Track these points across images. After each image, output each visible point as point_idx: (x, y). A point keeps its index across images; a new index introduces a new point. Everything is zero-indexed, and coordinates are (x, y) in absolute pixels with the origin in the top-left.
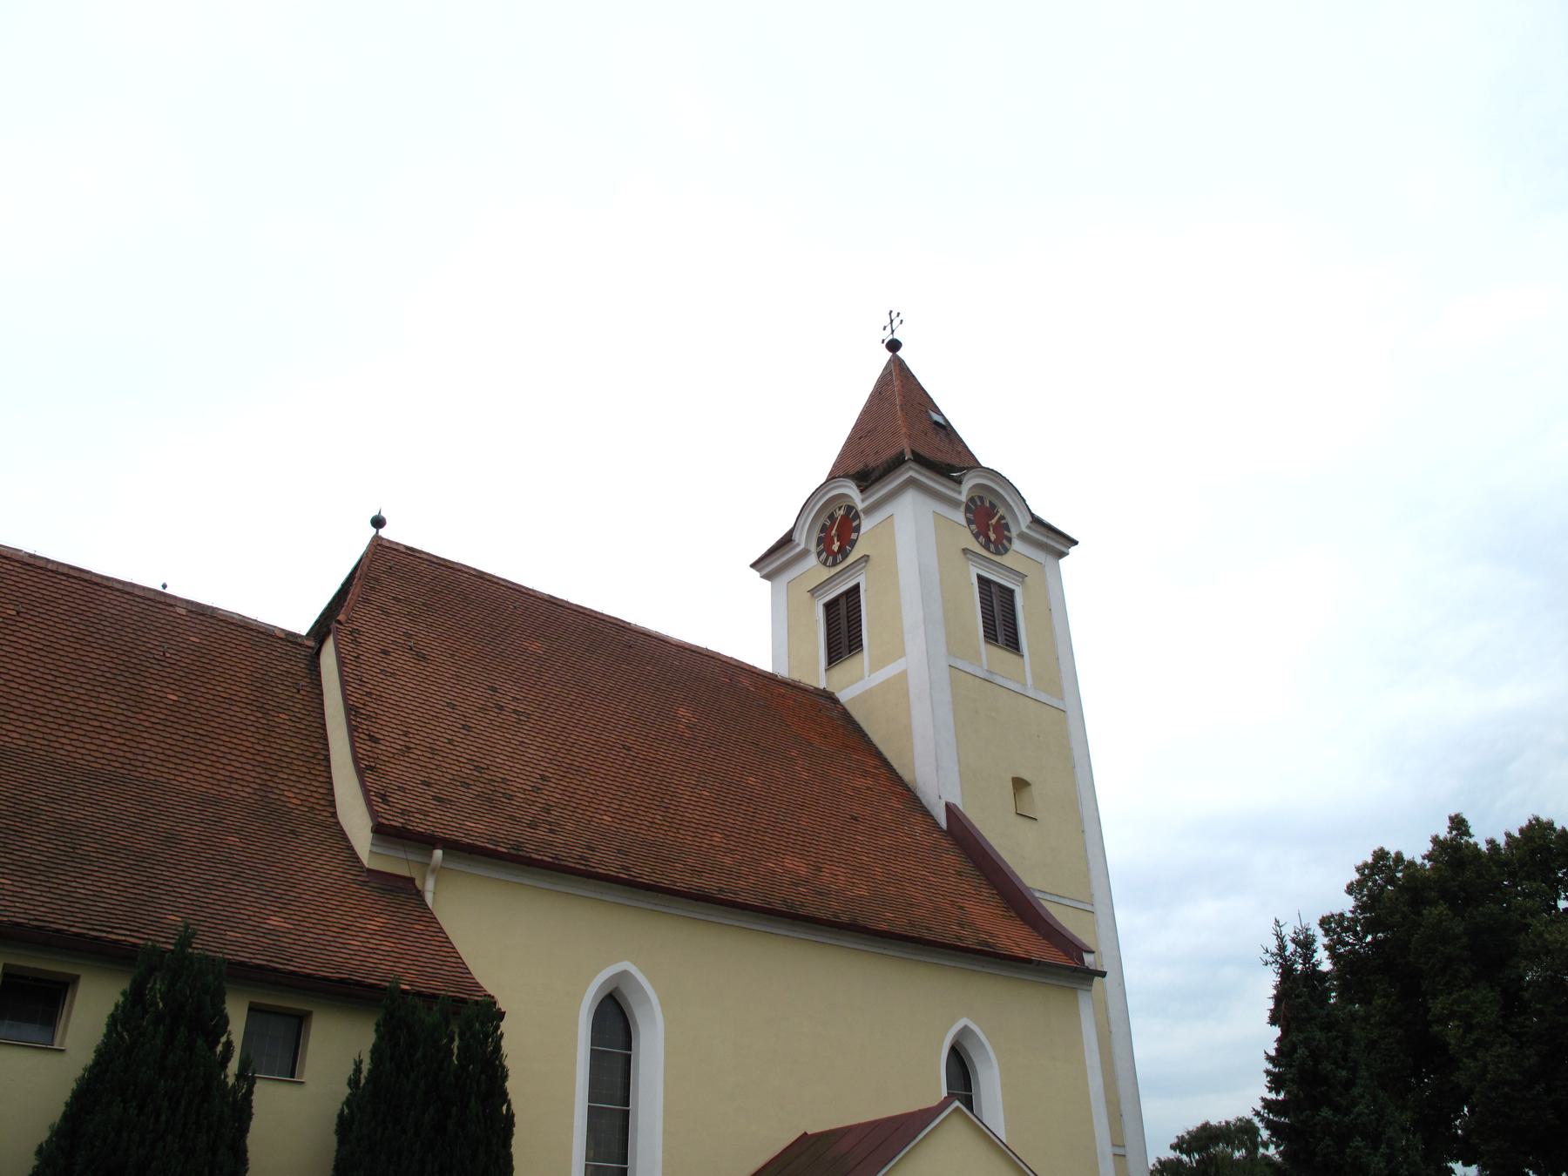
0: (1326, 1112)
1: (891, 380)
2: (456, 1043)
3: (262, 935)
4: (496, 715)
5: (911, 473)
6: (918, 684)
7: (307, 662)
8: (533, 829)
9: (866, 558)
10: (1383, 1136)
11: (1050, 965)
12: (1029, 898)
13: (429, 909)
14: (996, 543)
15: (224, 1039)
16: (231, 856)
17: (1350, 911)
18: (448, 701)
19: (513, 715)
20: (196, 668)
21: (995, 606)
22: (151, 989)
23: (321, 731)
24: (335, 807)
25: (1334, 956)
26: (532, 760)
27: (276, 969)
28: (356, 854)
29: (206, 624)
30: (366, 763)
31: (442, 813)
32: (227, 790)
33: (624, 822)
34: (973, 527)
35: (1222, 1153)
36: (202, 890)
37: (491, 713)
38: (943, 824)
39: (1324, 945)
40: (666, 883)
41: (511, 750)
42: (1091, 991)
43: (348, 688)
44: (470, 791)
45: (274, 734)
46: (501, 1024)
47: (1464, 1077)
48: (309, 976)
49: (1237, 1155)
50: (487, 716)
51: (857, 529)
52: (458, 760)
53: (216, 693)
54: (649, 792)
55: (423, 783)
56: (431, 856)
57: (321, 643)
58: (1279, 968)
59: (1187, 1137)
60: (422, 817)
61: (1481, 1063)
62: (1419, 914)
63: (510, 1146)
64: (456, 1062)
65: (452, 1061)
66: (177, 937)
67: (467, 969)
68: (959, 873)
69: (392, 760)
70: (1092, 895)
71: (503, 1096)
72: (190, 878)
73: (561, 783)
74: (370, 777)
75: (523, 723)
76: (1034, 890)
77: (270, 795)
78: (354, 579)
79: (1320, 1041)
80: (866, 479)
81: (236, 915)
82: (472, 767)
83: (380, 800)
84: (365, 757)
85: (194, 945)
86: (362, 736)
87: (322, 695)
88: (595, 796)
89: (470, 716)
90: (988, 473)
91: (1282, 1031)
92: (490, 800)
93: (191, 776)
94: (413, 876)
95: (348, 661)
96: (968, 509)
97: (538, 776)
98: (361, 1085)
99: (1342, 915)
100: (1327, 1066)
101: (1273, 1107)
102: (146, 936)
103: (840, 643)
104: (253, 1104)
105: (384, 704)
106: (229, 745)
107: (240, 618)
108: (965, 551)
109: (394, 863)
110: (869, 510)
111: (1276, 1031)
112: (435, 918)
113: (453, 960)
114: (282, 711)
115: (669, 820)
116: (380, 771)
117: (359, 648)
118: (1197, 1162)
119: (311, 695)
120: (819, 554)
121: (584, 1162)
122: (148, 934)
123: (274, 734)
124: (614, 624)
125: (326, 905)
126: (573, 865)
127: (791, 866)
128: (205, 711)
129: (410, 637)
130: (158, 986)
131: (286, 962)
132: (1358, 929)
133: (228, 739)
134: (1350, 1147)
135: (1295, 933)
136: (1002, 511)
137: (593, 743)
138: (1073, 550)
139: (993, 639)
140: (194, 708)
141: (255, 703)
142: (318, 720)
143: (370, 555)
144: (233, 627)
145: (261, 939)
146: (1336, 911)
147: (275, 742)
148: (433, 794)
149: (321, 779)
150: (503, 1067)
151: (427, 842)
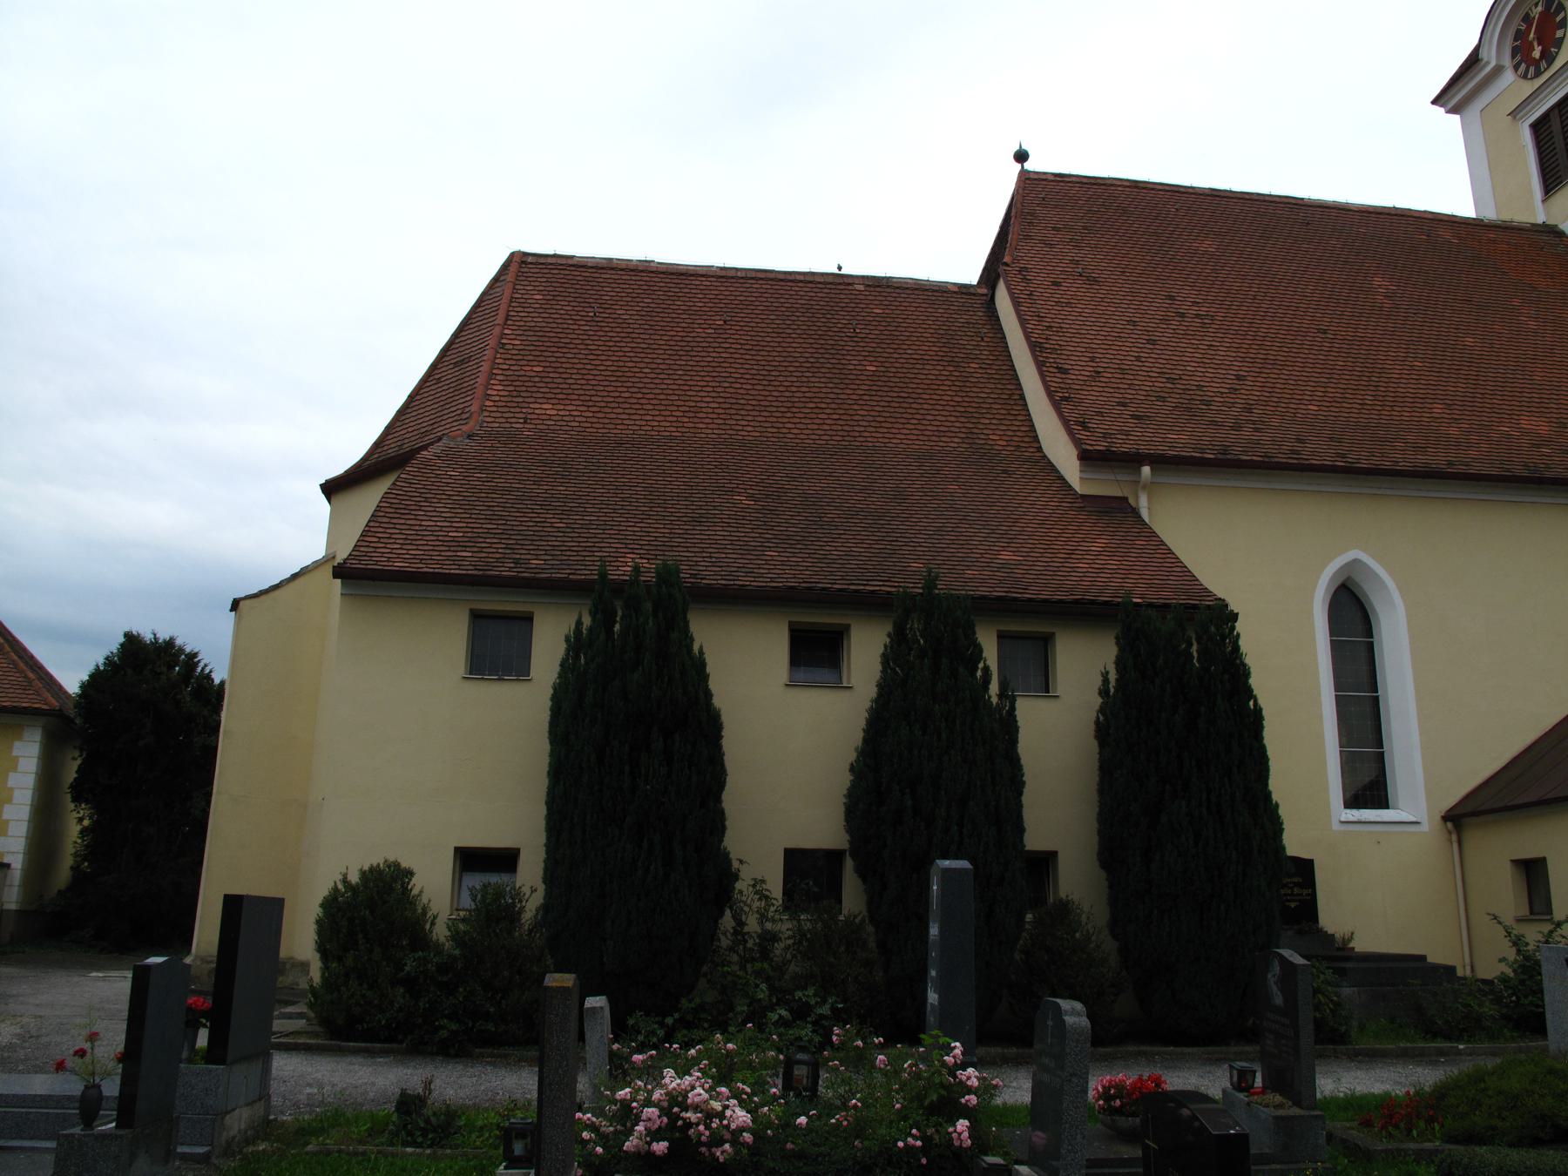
2: (1195, 647)
13: (1146, 524)
15: (981, 665)
24: (1039, 442)
27: (1015, 599)
28: (1067, 482)
40: (1387, 464)
44: (1166, 404)
45: (968, 384)
50: (1170, 326)
55: (1119, 404)
56: (1139, 472)
57: (993, 288)
60: (1124, 437)
63: (1262, 738)
64: (1197, 665)
66: (923, 581)
69: (1085, 387)
71: (1249, 693)
75: (1208, 326)
82: (1164, 380)
83: (1080, 428)
85: (939, 587)
86: (1051, 369)
98: (1111, 694)
102: (896, 584)
104: (1018, 719)
109: (1105, 485)
112: (1154, 532)
113: (1179, 569)
115: (1381, 398)
117: (1031, 285)
119: (994, 340)
120: (1516, 68)
123: (968, 384)
126: (1284, 460)
130: (915, 625)
143: (1021, 191)
145: (997, 574)
151: (1132, 461)
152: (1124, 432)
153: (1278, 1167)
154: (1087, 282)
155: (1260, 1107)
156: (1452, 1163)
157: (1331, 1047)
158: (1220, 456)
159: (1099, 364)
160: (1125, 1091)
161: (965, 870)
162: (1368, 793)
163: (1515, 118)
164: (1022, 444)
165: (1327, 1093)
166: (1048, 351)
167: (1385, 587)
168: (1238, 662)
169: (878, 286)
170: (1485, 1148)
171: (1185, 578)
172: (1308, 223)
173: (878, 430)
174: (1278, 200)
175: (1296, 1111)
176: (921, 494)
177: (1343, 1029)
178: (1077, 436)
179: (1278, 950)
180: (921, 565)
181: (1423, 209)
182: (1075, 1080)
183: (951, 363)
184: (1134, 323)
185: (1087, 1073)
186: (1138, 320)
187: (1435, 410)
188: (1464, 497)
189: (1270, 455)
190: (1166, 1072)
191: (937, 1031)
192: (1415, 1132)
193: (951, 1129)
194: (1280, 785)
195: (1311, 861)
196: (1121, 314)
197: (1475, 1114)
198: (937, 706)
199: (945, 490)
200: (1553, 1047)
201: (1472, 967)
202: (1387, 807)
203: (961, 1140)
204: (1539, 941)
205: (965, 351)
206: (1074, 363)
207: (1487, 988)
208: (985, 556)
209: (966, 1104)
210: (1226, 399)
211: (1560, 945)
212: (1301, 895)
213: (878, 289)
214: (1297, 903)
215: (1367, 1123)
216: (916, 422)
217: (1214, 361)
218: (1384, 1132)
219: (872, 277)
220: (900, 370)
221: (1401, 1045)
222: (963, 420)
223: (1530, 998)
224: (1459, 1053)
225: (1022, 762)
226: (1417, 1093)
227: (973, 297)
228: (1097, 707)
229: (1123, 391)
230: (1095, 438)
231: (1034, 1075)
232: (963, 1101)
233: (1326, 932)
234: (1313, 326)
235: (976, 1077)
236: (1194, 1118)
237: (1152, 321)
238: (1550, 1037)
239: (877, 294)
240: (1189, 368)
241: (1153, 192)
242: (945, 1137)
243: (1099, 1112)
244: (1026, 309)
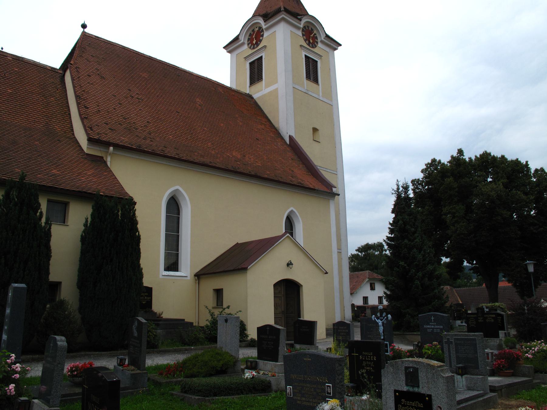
0: (406, 241)
5: (283, 16)
6: (281, 93)
7: (60, 79)
8: (145, 140)
9: (265, 47)
10: (423, 249)
13: (109, 167)
15: (39, 211)
17: (422, 178)
18: (113, 94)
19: (137, 100)
21: (310, 67)
22: (12, 194)
23: (67, 104)
24: (73, 132)
25: (415, 192)
27: (56, 188)
30: (84, 116)
32: (33, 125)
35: (372, 252)
37: (129, 99)
38: (288, 142)
39: (412, 189)
41: (137, 112)
42: (334, 200)
43: (76, 88)
44: (122, 126)
46: (135, 206)
47: (450, 232)
48: (68, 190)
49: (376, 253)
51: (263, 36)
52: (117, 116)
53: (26, 90)
55: (105, 123)
56: (109, 149)
57: (65, 71)
58: (396, 195)
60: (105, 135)
61: (456, 228)
62: (444, 180)
63: (139, 246)
64: (120, 219)
65: (119, 218)
66: (20, 177)
67: (123, 188)
68: (292, 159)
69: (94, 115)
70: (337, 169)
71: (137, 230)
73: (155, 124)
74: (86, 121)
75: (141, 102)
78: (76, 48)
79: (407, 219)
80: (267, 17)
81: (40, 169)
82: (123, 118)
83: (90, 129)
84: (84, 114)
85: (26, 179)
87: (66, 91)
89: (121, 100)
90: (312, 17)
91: (395, 215)
94: (103, 156)
96: (303, 31)
97: (146, 122)
99: (419, 179)
100: (408, 227)
101: (390, 239)
102: (9, 176)
103: (255, 77)
104: (52, 232)
105: (89, 95)
106: (33, 109)
107: (33, 62)
108: (301, 46)
109: (96, 151)
110: (267, 29)
111: (393, 215)
113: (118, 185)
118: (364, 255)
119: (62, 91)
120: (248, 44)
122: (9, 176)
124: (173, 67)
126: (159, 153)
127: (235, 155)
128: (23, 97)
129: (98, 70)
131: (59, 185)
132: (423, 184)
133: (32, 107)
134: (412, 252)
136: (315, 32)
137: (166, 110)
138: (339, 48)
139: (309, 79)
140: (18, 95)
141: (41, 94)
142: (66, 100)
143: (81, 39)
144: (31, 65)
146: (417, 178)
147: (50, 108)
149: (67, 122)
151: (107, 144)
152: (105, 134)
153: (131, 391)
154: (101, 78)
155: (126, 371)
157: (152, 349)
158: (137, 148)
159: (100, 108)
160: (79, 368)
161: (23, 288)
162: (172, 266)
163: (245, 59)
165: (149, 365)
166: (82, 99)
169: (18, 60)
170: (196, 378)
173: (9, 116)
174: (171, 66)
175: (139, 371)
176: (24, 143)
177: (156, 344)
178: (88, 132)
179: (137, 318)
180: (20, 170)
181: (215, 80)
182: (59, 365)
183: (43, 96)
184: (115, 96)
185: (65, 363)
186: (117, 95)
187: (209, 145)
189: (154, 150)
192: (176, 375)
193: (7, 389)
194: (144, 262)
195: (152, 288)
198: (19, 225)
199: (34, 143)
200: (218, 346)
202: (178, 271)
203: (11, 392)
204: (218, 314)
205: (50, 93)
206: (91, 105)
208: (46, 170)
209: (14, 378)
210: (143, 129)
211: (224, 315)
212: (147, 299)
215: (161, 374)
216: (26, 115)
218: (166, 376)
219: (16, 55)
221: (174, 348)
222: (45, 118)
224: (192, 349)
225: (52, 248)
226: (177, 363)
227: (56, 73)
228: (82, 230)
229: (108, 119)
230: (94, 134)
231: (44, 365)
232: (13, 377)
233: (154, 312)
234: (175, 110)
235: (20, 367)
236: (102, 376)
238: (218, 343)
239: (17, 63)
242: (4, 392)
243: (68, 377)
244: (76, 82)
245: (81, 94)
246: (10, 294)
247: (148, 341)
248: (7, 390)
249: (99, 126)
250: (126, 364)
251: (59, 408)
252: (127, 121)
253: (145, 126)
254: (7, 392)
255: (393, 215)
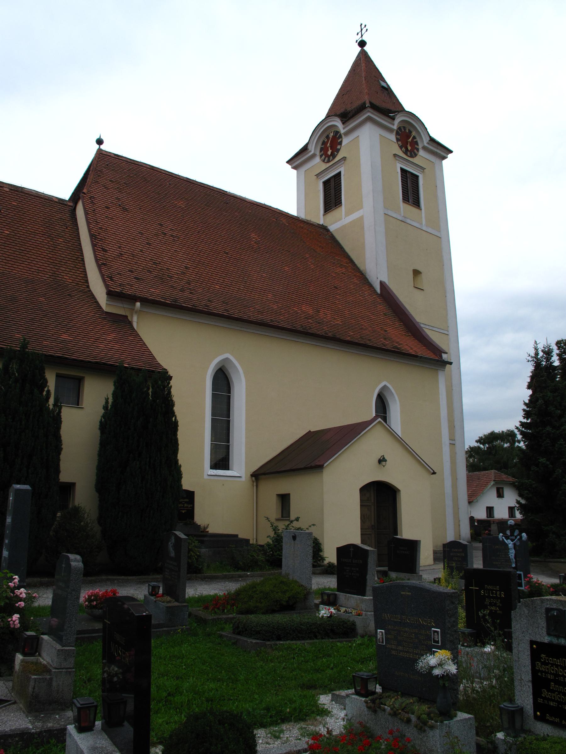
0: (549, 428)
1: (360, 63)
2: (151, 390)
3: (59, 343)
4: (163, 238)
5: (369, 114)
6: (368, 222)
9: (344, 159)
11: (426, 358)
12: (418, 327)
13: (135, 330)
14: (410, 151)
15: (46, 389)
16: (42, 307)
20: (17, 218)
23: (79, 247)
25: (561, 359)
26: (181, 259)
27: (67, 358)
28: (99, 305)
29: (19, 196)
31: (139, 285)
32: (37, 276)
33: (225, 289)
34: (400, 143)
36: (30, 323)
37: (160, 237)
38: (379, 291)
39: (557, 354)
40: (245, 317)
41: (170, 255)
44: (152, 274)
45: (57, 249)
48: (82, 361)
49: (506, 445)
50: (158, 238)
51: (340, 143)
54: (237, 274)
56: (135, 305)
57: (76, 204)
58: (534, 363)
59: (483, 437)
60: (130, 287)
63: (177, 435)
66: (20, 344)
67: (154, 357)
68: (385, 314)
69: (114, 260)
72: (24, 318)
74: (104, 269)
76: (421, 323)
77: (57, 278)
80: (345, 117)
82: (152, 263)
83: (109, 279)
85: (29, 348)
86: (99, 249)
87: (78, 229)
88: (212, 276)
91: (532, 392)
92: (161, 279)
93: (20, 270)
95: (90, 213)
96: (397, 133)
98: (109, 409)
102: (7, 344)
103: (331, 201)
107: (36, 192)
108: (395, 155)
109: (118, 309)
111: (530, 392)
112: (138, 334)
113: (148, 353)
114: (60, 238)
115: (247, 288)
116: (108, 265)
117: (95, 206)
118: (487, 448)
120: (321, 156)
121: (210, 442)
123: (57, 249)
125: (87, 329)
126: (202, 309)
128: (23, 239)
129: (119, 200)
130: (14, 367)
133: (35, 252)
135: (544, 347)
136: (414, 134)
138: (450, 156)
139: (407, 201)
140: (17, 237)
143: (97, 159)
144: (33, 197)
145: (59, 345)
148: (134, 276)
150: (172, 401)
151: (132, 299)
155: (160, 602)
156: (239, 622)
157: (195, 575)
160: (99, 597)
163: (317, 177)
164: (79, 283)
165: (191, 595)
166: (99, 239)
167: (239, 372)
168: (170, 399)
170: (253, 615)
171: (150, 357)
172: (227, 203)
175: (176, 604)
176: (25, 300)
177: (200, 567)
178: (107, 283)
179: (174, 532)
180: (21, 336)
184: (142, 234)
185: (80, 589)
188: (225, 326)
189: (196, 305)
190: (119, 588)
191: (6, 570)
192: (226, 611)
193: (10, 619)
194: (183, 457)
195: (193, 492)
196: (136, 228)
197: (250, 602)
200: (283, 573)
201: (256, 540)
202: (228, 469)
203: (15, 625)
204: (284, 529)
207: (261, 548)
209: (18, 606)
210: (180, 277)
213: (16, 193)
214: (186, 511)
215: (206, 608)
217: (176, 258)
218: (213, 611)
220: (22, 236)
221: (224, 573)
223: (278, 552)
224: (248, 576)
225: (62, 438)
226: (228, 593)
230: (116, 286)
231: (54, 591)
232: (17, 605)
235: (25, 593)
237: (100, 218)
240: (164, 259)
241: (160, 173)
243: (86, 608)
244: (91, 217)
245: (98, 232)
246: (11, 498)
247: (188, 563)
248: (10, 621)
249: (122, 275)
250: (160, 593)
251: (74, 648)
252: (158, 267)
253: (183, 273)
254: (10, 624)
255: (530, 392)
